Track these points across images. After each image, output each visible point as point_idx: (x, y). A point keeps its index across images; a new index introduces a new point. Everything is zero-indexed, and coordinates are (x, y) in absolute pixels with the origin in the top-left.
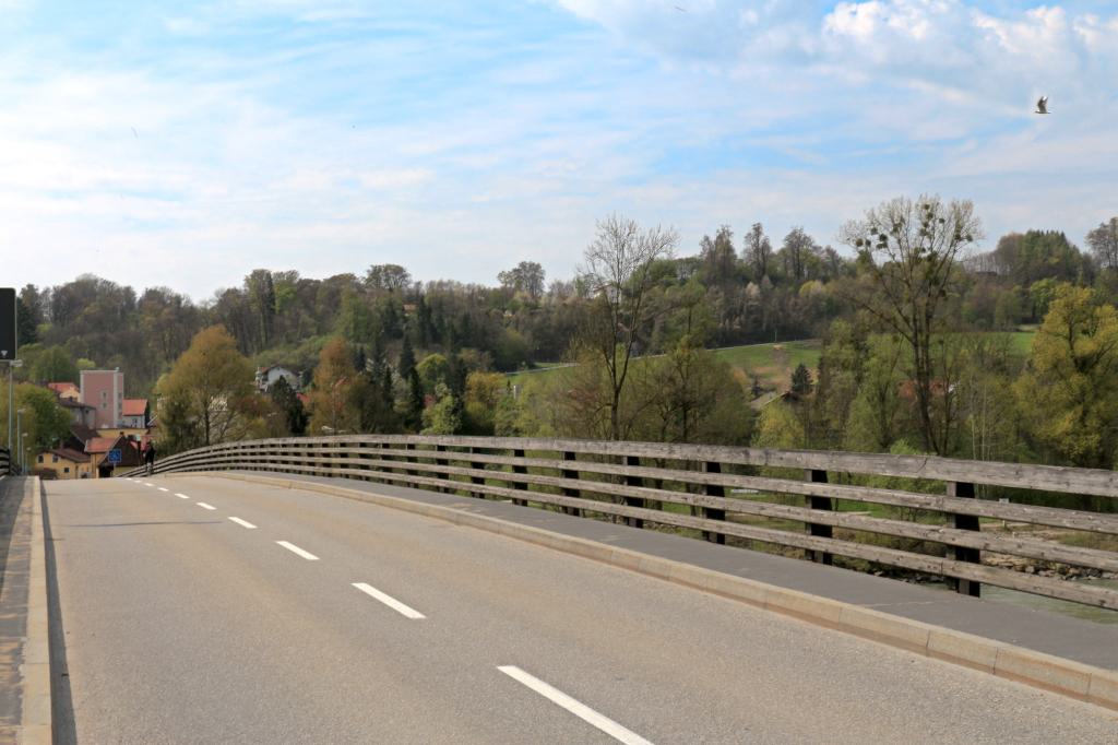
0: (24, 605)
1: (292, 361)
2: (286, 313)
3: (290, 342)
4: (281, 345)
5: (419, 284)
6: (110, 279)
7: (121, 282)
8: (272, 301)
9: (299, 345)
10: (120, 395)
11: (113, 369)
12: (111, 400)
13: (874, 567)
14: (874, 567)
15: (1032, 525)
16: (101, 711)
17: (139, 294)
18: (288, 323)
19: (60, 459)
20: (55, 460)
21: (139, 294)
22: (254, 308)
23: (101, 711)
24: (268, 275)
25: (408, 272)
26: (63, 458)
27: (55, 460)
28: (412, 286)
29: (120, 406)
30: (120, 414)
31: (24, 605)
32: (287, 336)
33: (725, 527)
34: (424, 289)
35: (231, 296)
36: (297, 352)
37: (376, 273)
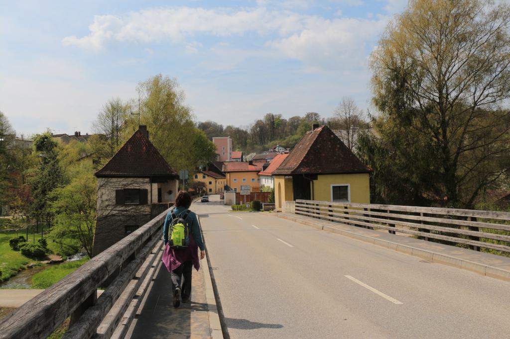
0: (304, 175)
1: (283, 145)
2: (280, 128)
3: (281, 138)
4: (278, 139)
5: (324, 119)
6: (216, 122)
7: (219, 123)
8: (274, 124)
9: (285, 139)
10: (230, 149)
11: (227, 136)
12: (227, 152)
13: (356, 225)
14: (356, 225)
15: (482, 213)
16: (81, 208)
17: (224, 128)
18: (280, 131)
19: (206, 176)
20: (204, 177)
21: (224, 128)
22: (268, 127)
23: (81, 208)
24: (273, 115)
25: (319, 115)
26: (208, 176)
27: (204, 177)
28: (321, 120)
29: (230, 154)
30: (231, 158)
31: (304, 175)
32: (280, 136)
33: (320, 216)
34: (326, 121)
35: (260, 122)
36: (285, 141)
37: (308, 116)
